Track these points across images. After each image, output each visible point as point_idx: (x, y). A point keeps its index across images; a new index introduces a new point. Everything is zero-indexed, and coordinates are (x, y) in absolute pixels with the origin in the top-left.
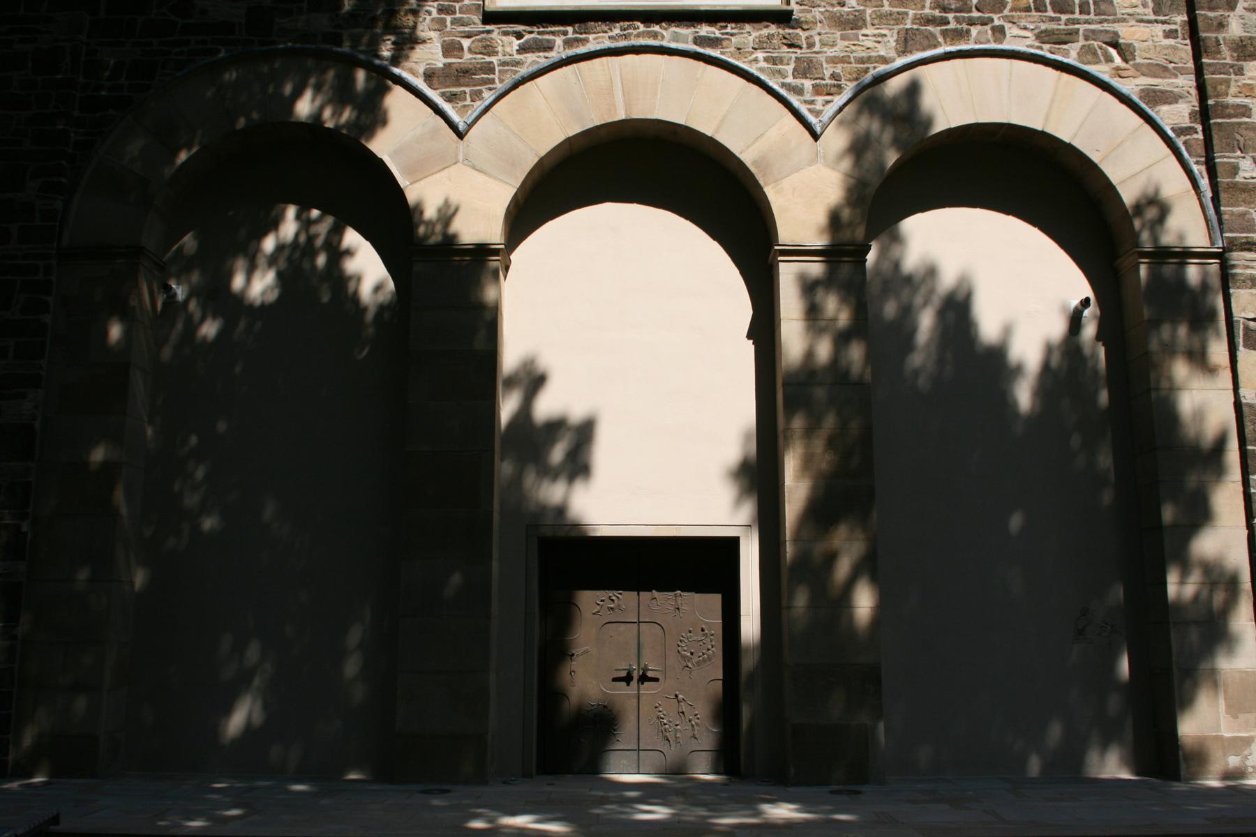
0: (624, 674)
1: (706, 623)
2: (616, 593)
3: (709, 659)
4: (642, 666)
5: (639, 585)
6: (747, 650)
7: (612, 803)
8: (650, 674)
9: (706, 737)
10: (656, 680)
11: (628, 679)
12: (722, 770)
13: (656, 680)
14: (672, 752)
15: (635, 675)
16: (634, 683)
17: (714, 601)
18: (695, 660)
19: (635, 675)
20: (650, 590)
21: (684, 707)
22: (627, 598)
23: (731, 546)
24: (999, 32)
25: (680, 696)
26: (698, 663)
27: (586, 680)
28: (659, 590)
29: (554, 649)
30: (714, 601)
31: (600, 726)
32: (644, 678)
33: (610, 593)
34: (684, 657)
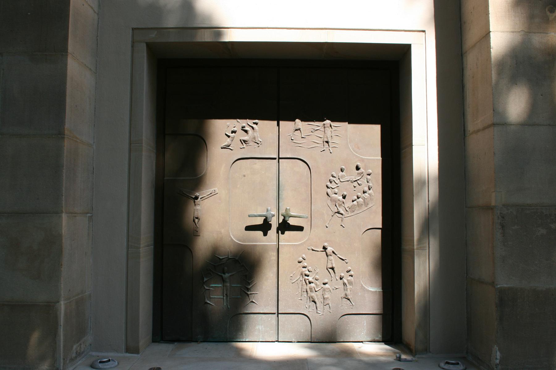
0: (259, 221)
1: (362, 160)
2: (250, 122)
3: (366, 203)
4: (282, 211)
5: (279, 113)
6: (423, 183)
7: (368, 291)
8: (292, 222)
9: (367, 293)
10: (300, 229)
11: (265, 227)
12: (379, 337)
13: (300, 229)
14: (321, 317)
15: (274, 224)
16: (273, 232)
17: (372, 133)
18: (348, 203)
19: (274, 224)
20: (293, 120)
21: (334, 261)
22: (265, 129)
23: (393, 62)
24: (274, 216)
25: (330, 250)
26: (352, 209)
27: (221, 214)
28: (303, 120)
29: (178, 180)
30: (372, 133)
31: (241, 268)
32: (284, 227)
33: (243, 122)
34: (334, 201)
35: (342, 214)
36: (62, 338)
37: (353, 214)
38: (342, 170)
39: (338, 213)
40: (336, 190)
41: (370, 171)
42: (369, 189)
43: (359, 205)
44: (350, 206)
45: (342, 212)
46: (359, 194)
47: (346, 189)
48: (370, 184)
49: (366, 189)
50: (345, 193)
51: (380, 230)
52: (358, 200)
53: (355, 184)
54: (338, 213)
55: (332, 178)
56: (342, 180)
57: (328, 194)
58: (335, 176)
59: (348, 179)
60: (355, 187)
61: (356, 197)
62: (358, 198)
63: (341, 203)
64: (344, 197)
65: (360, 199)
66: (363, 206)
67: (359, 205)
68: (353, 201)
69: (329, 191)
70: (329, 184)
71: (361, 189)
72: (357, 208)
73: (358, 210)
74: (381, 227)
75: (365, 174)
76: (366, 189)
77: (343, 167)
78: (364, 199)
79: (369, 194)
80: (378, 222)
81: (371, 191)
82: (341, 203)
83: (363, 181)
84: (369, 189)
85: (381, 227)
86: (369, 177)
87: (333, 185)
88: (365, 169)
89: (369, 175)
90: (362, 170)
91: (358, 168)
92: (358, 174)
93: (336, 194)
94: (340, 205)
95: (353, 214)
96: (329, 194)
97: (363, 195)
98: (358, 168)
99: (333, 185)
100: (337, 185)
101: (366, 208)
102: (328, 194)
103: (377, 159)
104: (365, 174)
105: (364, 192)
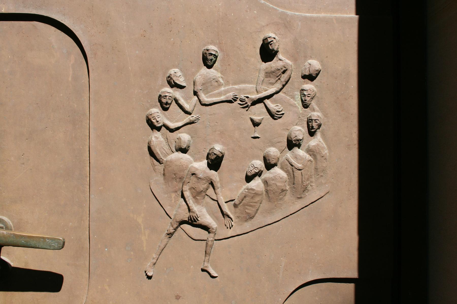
1: (286, 24)
3: (298, 187)
10: (50, 282)
18: (229, 185)
26: (245, 207)
34: (176, 177)
35: (206, 228)
36: (294, 161)
37: (247, 226)
38: (208, 61)
39: (193, 222)
40: (184, 137)
41: (315, 64)
42: (312, 133)
43: (272, 194)
44: (236, 196)
45: (206, 218)
46: (273, 151)
47: (224, 131)
48: (316, 114)
49: (299, 131)
50: (218, 148)
51: (351, 286)
52: (267, 175)
53: (258, 113)
54: (193, 222)
55: (168, 90)
56: (206, 99)
57: (152, 153)
58: (181, 81)
59: (230, 96)
60: (256, 124)
61: (259, 164)
62: (269, 166)
63: (202, 186)
64: (215, 163)
65: (277, 170)
66: (288, 197)
67: (272, 194)
68: (249, 179)
69: (157, 138)
70: (156, 111)
71: (279, 130)
72: (265, 205)
73: (270, 212)
74: (354, 274)
75: (296, 77)
76: (299, 131)
77: (213, 48)
78: (291, 169)
79: (310, 151)
80: (341, 249)
81: (314, 142)
82: (202, 186)
83: (288, 102)
84: (312, 133)
85: (354, 274)
86: (309, 86)
87: (174, 118)
88: (295, 59)
89: (311, 77)
90: (282, 60)
91: (267, 53)
92: (269, 74)
93: (184, 151)
94: (198, 194)
95: (247, 226)
96: (157, 151)
97: (289, 154)
98: (267, 53)
99: (174, 118)
100: (188, 118)
101: (299, 205)
102: (152, 153)
103: (341, 21)
104: (296, 77)
105: (292, 144)
